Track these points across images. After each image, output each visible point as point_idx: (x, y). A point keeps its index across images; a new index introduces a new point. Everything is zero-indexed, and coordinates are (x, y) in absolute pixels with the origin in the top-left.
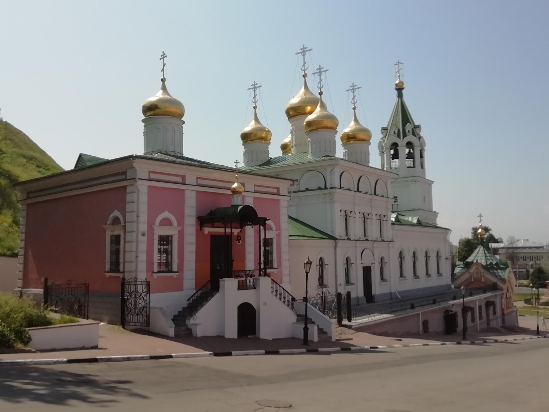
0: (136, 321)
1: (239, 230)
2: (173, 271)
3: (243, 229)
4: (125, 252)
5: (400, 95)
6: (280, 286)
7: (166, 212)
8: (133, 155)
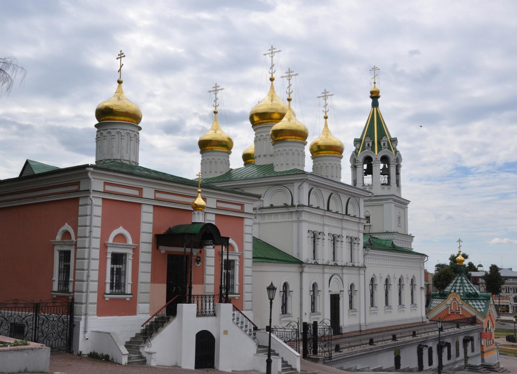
1: (198, 250)
2: (126, 293)
3: (202, 250)
4: (75, 269)
5: (375, 104)
6: (242, 313)
7: (121, 227)
8: (88, 164)
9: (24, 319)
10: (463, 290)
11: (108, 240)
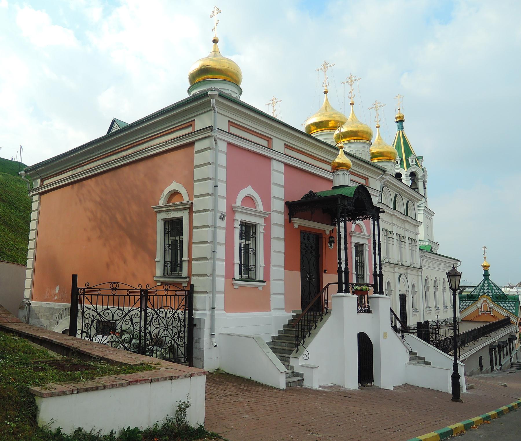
4: (190, 243)
9: (127, 314)
10: (492, 292)
11: (235, 203)
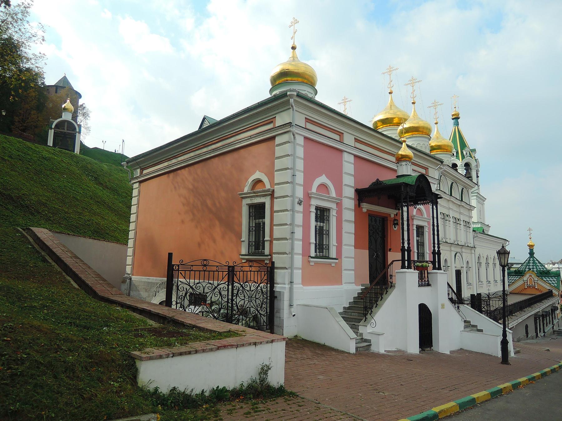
0: (202, 273)
9: (216, 287)
11: (311, 190)
